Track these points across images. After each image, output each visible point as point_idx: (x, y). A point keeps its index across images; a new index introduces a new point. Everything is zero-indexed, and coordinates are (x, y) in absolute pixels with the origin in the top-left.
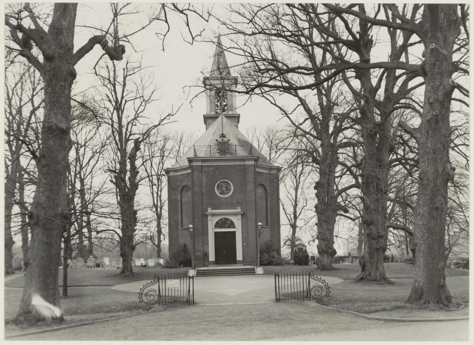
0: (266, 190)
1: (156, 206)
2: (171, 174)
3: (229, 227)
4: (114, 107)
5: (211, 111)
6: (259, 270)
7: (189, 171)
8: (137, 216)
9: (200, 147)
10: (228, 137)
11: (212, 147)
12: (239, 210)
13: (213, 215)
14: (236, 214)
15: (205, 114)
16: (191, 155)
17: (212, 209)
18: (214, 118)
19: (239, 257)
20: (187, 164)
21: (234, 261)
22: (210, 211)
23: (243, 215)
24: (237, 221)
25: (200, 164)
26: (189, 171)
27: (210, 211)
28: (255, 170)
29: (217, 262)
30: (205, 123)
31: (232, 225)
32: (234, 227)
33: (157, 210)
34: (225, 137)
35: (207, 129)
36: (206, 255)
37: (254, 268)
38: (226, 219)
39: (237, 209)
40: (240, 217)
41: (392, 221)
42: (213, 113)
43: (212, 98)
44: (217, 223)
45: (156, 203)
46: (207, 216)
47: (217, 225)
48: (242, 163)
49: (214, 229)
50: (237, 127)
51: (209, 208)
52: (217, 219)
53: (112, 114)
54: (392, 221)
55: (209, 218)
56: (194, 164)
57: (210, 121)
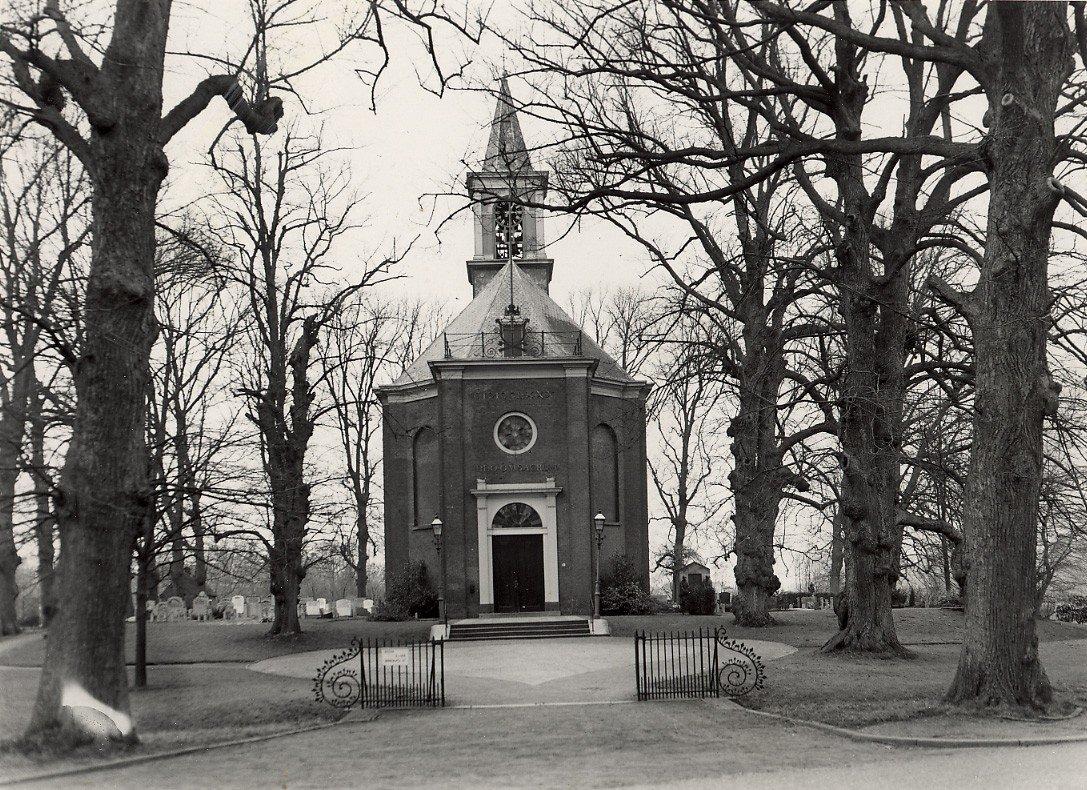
2: (392, 400)
3: (526, 525)
5: (485, 252)
6: (599, 626)
7: (434, 393)
8: (309, 499)
12: (550, 484)
13: (490, 496)
14: (543, 495)
16: (438, 355)
18: (493, 268)
19: (551, 594)
22: (481, 486)
23: (560, 496)
24: (546, 511)
25: (458, 376)
26: (434, 393)
27: (481, 486)
28: (588, 390)
29: (499, 607)
31: (534, 519)
33: (357, 484)
34: (517, 312)
36: (473, 590)
40: (552, 501)
45: (355, 469)
46: (474, 498)
47: (499, 520)
52: (497, 506)
53: (252, 260)
55: (481, 503)
56: (444, 376)
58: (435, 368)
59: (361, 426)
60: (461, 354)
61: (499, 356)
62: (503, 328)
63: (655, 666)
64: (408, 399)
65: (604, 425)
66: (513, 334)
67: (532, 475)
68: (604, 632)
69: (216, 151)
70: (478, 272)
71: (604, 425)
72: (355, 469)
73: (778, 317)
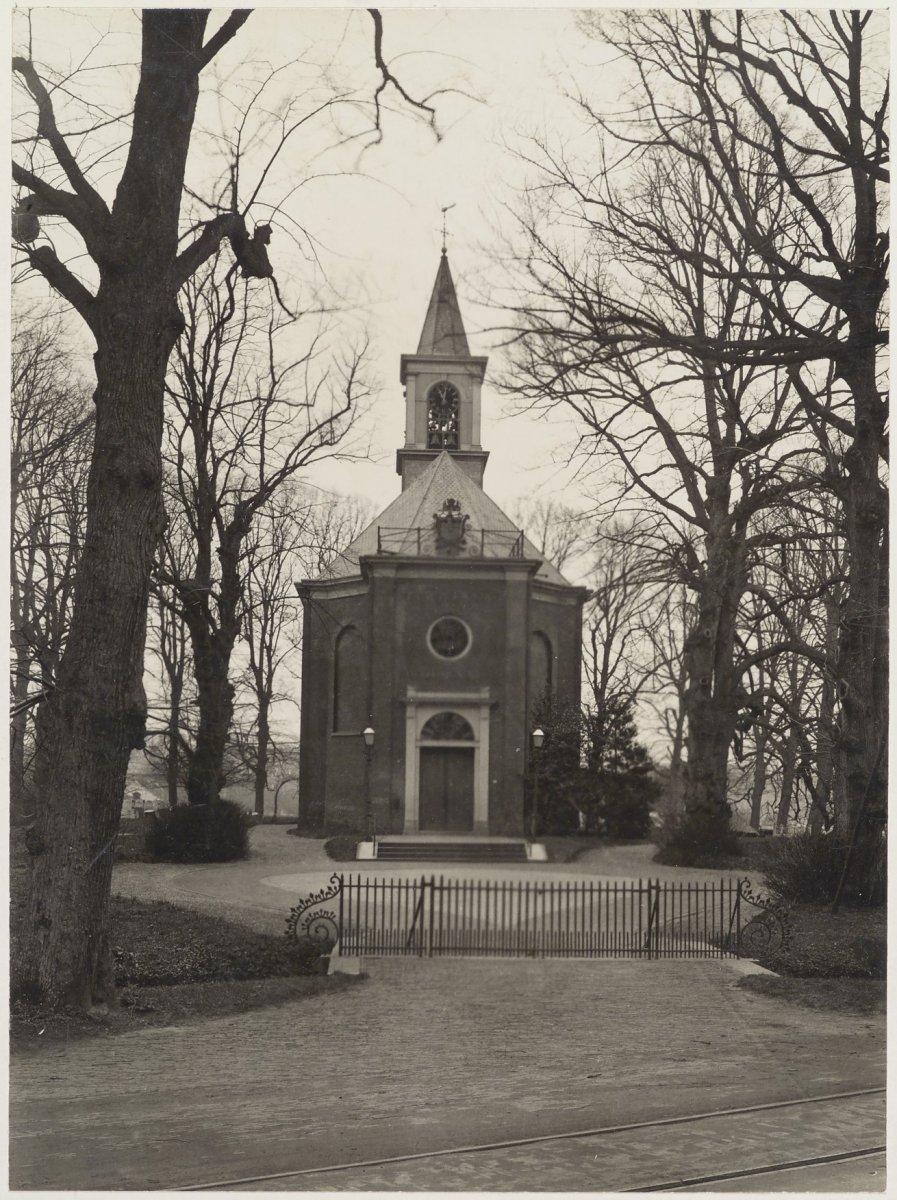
0: (548, 644)
1: (258, 672)
2: (316, 596)
3: (458, 737)
4: (187, 419)
5: (418, 441)
6: (537, 852)
7: (364, 590)
8: (233, 701)
9: (392, 531)
10: (466, 510)
11: (422, 533)
12: (485, 694)
13: (422, 704)
14: (475, 705)
15: (401, 446)
16: (369, 548)
17: (418, 690)
18: (427, 458)
19: (481, 813)
20: (357, 571)
21: (467, 823)
22: (411, 693)
23: (494, 707)
24: (481, 726)
25: (390, 573)
26: (364, 590)
27: (411, 693)
28: (529, 595)
29: (424, 824)
30: (400, 470)
31: (466, 731)
32: (471, 738)
33: (259, 683)
34: (457, 508)
35: (403, 489)
36: (397, 805)
37: (522, 846)
38: (450, 716)
39: (477, 691)
40: (485, 712)
41: (718, 372)
42: (422, 446)
43: (424, 406)
44: (428, 724)
45: (257, 665)
46: (403, 706)
47: (430, 730)
48: (494, 576)
49: (421, 740)
50: (480, 484)
51: (409, 687)
52: (425, 716)
53: (181, 437)
54: (718, 372)
55: (410, 711)
56: (379, 573)
57: (413, 464)
58: (366, 563)
59: (266, 620)
60: (392, 547)
61: (433, 553)
62: (439, 523)
63: (363, 908)
64: (334, 595)
65: (540, 634)
66: (450, 526)
67: (467, 684)
68: (371, 857)
69: (345, 407)
70: (406, 460)
71: (540, 634)
72: (257, 665)
73: (742, 528)
